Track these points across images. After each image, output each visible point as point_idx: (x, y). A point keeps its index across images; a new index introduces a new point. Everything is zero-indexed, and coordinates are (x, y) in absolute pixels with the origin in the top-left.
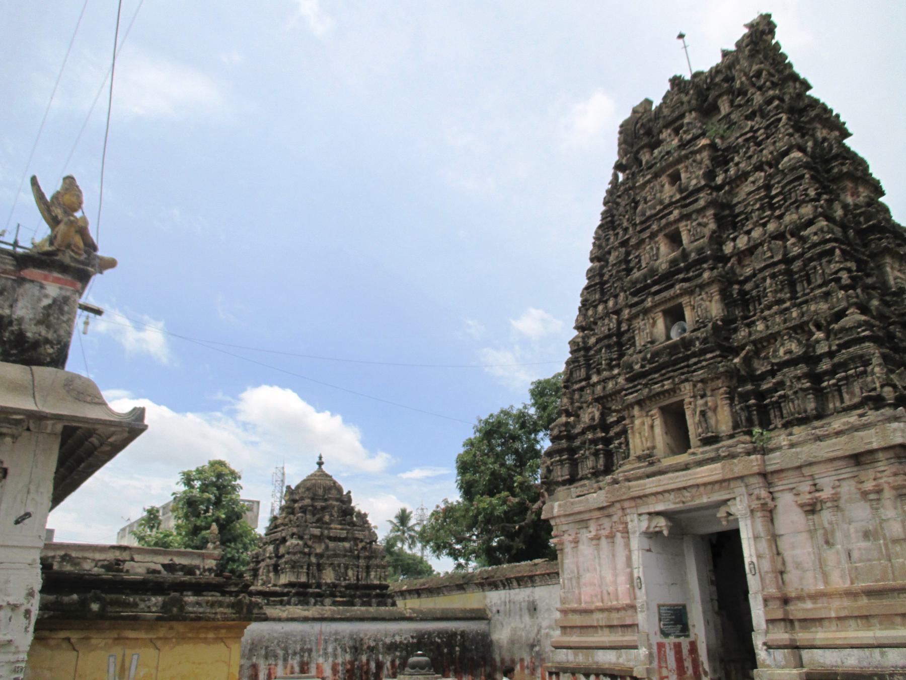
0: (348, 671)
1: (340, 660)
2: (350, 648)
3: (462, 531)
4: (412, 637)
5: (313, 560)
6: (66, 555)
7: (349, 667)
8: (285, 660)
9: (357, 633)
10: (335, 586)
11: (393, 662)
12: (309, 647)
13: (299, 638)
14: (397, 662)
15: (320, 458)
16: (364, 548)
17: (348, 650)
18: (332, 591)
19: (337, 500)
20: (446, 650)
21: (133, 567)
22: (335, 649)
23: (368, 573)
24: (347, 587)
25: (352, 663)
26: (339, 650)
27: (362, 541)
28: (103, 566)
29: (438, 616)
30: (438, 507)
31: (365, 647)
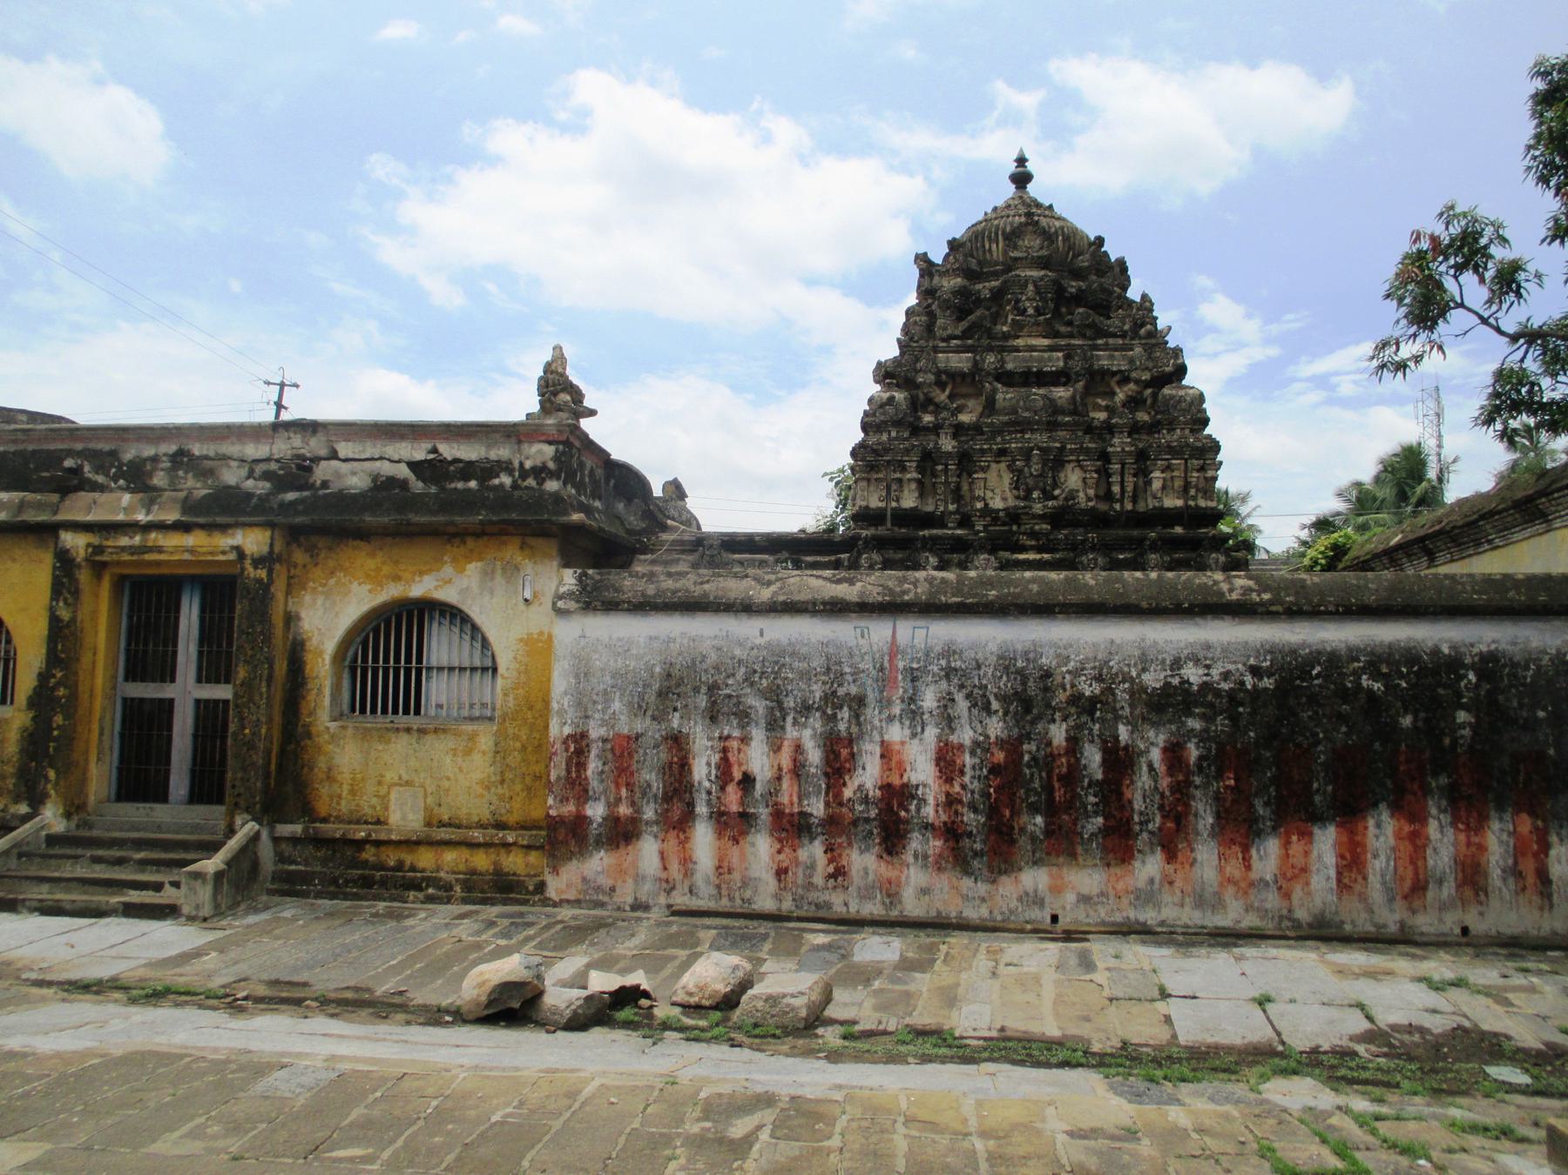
0: (995, 770)
1: (965, 735)
2: (1003, 699)
3: (1508, 281)
4: (1255, 671)
5: (947, 444)
6: (181, 452)
7: (1000, 756)
8: (774, 726)
9: (1031, 654)
10: (1013, 516)
11: (1173, 752)
12: (854, 690)
13: (817, 663)
14: (1193, 752)
15: (1021, 161)
16: (1134, 402)
17: (995, 705)
18: (1003, 537)
19: (1043, 263)
20: (1407, 721)
21: (338, 475)
22: (947, 701)
23: (1143, 473)
24: (1057, 518)
25: (1012, 746)
26: (962, 704)
27: (1125, 380)
28: (267, 476)
29: (1372, 599)
30: (1417, 237)
31: (1061, 697)
